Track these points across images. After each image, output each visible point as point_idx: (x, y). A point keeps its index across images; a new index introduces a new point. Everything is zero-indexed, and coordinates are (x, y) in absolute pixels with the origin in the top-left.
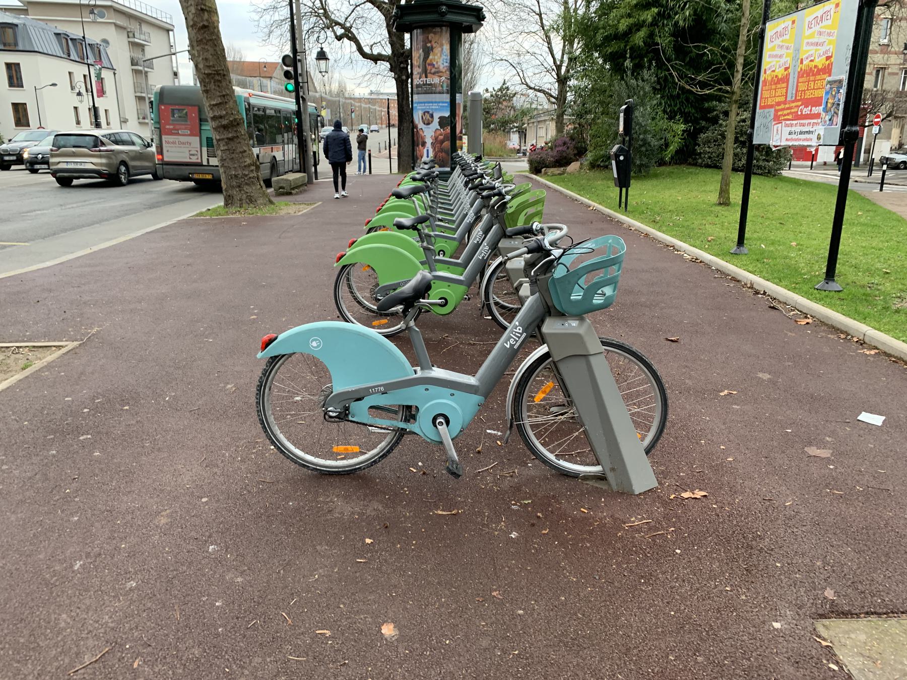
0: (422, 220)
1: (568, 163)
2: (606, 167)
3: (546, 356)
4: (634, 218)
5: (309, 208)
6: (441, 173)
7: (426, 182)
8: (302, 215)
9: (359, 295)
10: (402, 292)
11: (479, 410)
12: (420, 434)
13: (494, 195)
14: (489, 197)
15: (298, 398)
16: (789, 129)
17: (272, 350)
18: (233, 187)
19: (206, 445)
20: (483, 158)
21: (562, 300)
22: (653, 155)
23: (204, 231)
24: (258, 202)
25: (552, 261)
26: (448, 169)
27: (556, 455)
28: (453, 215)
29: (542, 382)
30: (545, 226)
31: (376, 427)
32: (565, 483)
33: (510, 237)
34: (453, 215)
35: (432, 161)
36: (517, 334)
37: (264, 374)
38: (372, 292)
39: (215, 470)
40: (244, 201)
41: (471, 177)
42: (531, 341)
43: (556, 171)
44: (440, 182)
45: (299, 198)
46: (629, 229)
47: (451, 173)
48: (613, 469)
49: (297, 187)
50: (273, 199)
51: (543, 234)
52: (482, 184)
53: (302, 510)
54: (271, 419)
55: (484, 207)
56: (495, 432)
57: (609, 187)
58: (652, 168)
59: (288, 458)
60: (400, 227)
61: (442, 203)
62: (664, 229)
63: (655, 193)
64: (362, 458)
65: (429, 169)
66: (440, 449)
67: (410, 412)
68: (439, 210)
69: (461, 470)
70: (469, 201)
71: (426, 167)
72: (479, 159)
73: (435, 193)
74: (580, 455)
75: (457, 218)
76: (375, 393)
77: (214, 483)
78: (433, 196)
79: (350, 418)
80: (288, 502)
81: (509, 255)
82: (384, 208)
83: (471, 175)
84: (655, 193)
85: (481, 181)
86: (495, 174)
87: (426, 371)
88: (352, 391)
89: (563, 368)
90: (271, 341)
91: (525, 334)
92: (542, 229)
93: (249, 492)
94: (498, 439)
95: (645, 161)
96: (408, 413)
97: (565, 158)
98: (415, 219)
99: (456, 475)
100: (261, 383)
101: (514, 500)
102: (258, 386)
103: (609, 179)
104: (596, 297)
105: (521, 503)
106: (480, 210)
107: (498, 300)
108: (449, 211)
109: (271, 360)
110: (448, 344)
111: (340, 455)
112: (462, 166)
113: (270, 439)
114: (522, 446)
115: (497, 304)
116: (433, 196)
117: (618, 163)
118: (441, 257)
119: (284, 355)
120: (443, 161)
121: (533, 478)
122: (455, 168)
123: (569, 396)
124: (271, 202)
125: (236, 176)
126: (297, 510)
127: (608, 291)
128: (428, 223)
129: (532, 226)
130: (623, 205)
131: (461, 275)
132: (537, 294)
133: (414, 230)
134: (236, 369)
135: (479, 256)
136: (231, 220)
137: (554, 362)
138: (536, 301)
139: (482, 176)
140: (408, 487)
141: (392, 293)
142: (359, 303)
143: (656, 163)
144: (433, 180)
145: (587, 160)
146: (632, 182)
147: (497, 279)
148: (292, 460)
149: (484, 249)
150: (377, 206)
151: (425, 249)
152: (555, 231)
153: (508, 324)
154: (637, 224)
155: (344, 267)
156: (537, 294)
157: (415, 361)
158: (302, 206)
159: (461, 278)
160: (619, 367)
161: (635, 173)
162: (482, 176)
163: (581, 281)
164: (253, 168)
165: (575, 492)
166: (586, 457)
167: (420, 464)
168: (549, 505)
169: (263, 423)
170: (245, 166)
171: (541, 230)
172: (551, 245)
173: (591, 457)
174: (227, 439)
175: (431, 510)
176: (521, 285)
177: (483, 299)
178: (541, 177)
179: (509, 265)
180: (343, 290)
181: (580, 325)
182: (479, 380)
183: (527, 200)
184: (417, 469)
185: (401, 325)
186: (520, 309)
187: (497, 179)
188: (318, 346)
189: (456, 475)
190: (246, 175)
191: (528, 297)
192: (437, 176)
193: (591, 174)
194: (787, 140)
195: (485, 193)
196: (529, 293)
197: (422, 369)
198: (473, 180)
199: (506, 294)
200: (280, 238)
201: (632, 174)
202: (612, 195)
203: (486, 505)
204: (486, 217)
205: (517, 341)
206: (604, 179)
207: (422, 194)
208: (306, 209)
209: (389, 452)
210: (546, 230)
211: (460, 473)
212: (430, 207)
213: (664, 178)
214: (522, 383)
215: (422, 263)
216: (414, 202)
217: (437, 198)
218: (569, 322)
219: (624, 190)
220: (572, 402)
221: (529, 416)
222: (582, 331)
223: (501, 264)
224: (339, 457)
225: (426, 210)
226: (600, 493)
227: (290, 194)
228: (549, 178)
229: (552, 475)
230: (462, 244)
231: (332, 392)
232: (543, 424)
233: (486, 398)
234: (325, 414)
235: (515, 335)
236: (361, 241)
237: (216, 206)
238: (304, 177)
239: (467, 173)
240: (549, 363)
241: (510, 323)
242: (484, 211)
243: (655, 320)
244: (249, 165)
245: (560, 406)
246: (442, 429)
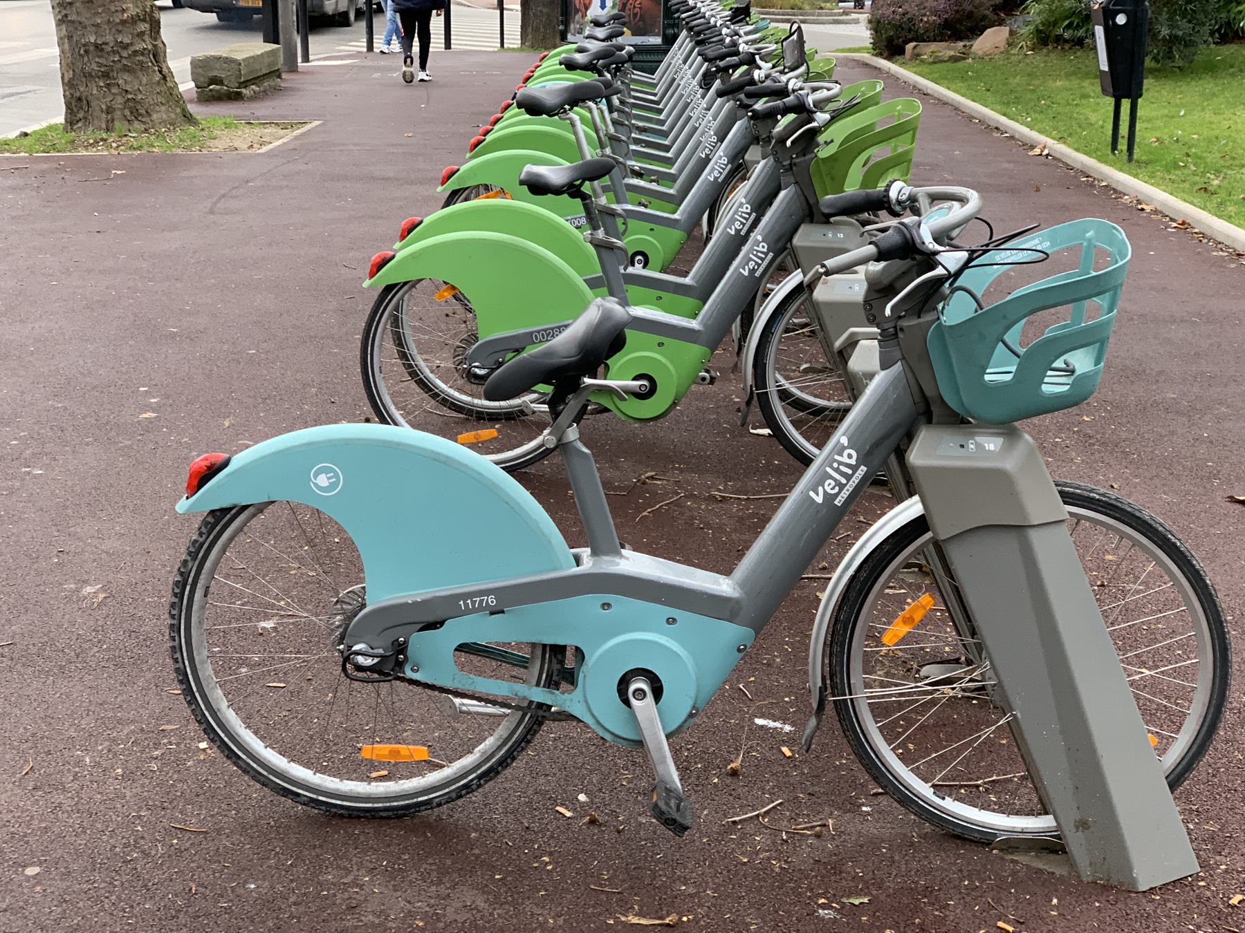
0: (596, 171)
1: (977, 30)
2: (1079, 42)
3: (918, 526)
4: (1151, 179)
5: (289, 136)
6: (640, 49)
7: (600, 74)
8: (269, 154)
9: (422, 364)
10: (548, 354)
11: (737, 669)
12: (588, 719)
13: (785, 111)
14: (770, 116)
15: (269, 624)
17: (216, 494)
18: (89, 76)
19: (34, 735)
20: (753, 10)
21: (960, 382)
22: (1206, 13)
23: (13, 189)
24: (155, 116)
25: (940, 281)
26: (656, 40)
27: (934, 786)
28: (670, 162)
29: (900, 602)
30: (921, 192)
31: (472, 697)
32: (959, 856)
33: (826, 219)
34: (670, 162)
35: (615, 18)
36: (843, 468)
37: (193, 555)
38: (460, 355)
39: (59, 798)
40: (118, 114)
41: (722, 64)
42: (872, 496)
43: (946, 49)
44: (638, 75)
45: (262, 109)
46: (1137, 207)
47: (663, 50)
48: (1082, 825)
49: (256, 80)
50: (192, 108)
51: (916, 212)
52: (752, 82)
53: (279, 902)
54: (207, 671)
55: (756, 140)
56: (778, 725)
57: (1085, 96)
58: (1203, 47)
59: (245, 771)
60: (538, 187)
61: (643, 130)
62: (1232, 209)
63: (1208, 115)
64: (434, 777)
65: (609, 38)
66: (634, 763)
67: (562, 662)
68: (633, 147)
69: (688, 813)
70: (715, 124)
71: (601, 33)
72: (741, 14)
73: (622, 102)
74: (998, 788)
75: (681, 170)
76: (474, 611)
77: (57, 830)
78: (619, 110)
79: (409, 674)
80: (246, 882)
81: (830, 263)
82: (489, 138)
83: (722, 58)
84: (1208, 115)
85: (748, 72)
86: (788, 55)
87: (606, 558)
88: (415, 603)
89: (958, 557)
90: (213, 470)
91: (863, 468)
92: (913, 199)
93: (145, 854)
94: (784, 743)
95: (1184, 28)
96: (556, 666)
97: (970, 15)
98: (575, 168)
99: (679, 828)
100: (184, 575)
101: (823, 895)
102: (177, 583)
103: (1086, 75)
104: (1051, 377)
105: (843, 905)
106: (744, 150)
107: (786, 385)
108: (658, 148)
109: (210, 519)
110: (655, 497)
111: (376, 769)
112: (698, 34)
113: (202, 720)
114: (846, 759)
115: (784, 395)
116: (619, 110)
117: (1111, 31)
118: (637, 269)
119: (245, 507)
120: (642, 18)
121: (875, 843)
122: (675, 37)
123: (973, 633)
124: (189, 118)
125: (98, 47)
126: (269, 903)
127: (1081, 361)
128: (606, 180)
129: (887, 190)
130: (1123, 145)
131: (695, 316)
132: (898, 367)
133: (573, 196)
134: (108, 545)
135: (740, 267)
136: (83, 163)
137: (938, 545)
138: (894, 384)
139: (750, 61)
140: (551, 854)
141: (531, 351)
142: (424, 385)
143: (1212, 34)
144: (618, 69)
145: (1027, 23)
146: (1148, 83)
147: (787, 331)
148: (256, 776)
149: (756, 252)
150: (473, 135)
151: (599, 246)
152: (947, 204)
153: (815, 450)
154: (1158, 195)
155: (389, 288)
156: (898, 367)
157: (576, 533)
158: (269, 130)
159: (694, 324)
160: (1103, 566)
161: (1155, 59)
162: (750, 61)
163: (1013, 336)
164: (144, 27)
165: (983, 881)
166: (1014, 793)
167: (582, 797)
168: (916, 910)
169: (184, 680)
170: (123, 22)
171: (912, 205)
172: (937, 239)
173: (1027, 795)
174: (87, 723)
175: (611, 914)
176: (852, 343)
177: (750, 380)
178: (902, 65)
179: (820, 294)
180: (384, 352)
181: (1007, 448)
182: (742, 585)
183: (871, 127)
184: (574, 810)
185: (546, 437)
186: (847, 411)
187: (793, 69)
188: (332, 486)
189: (679, 828)
190: (126, 47)
191: (871, 376)
192: (630, 55)
193: (1038, 59)
195: (760, 105)
196: (875, 363)
197: (595, 553)
198: (725, 70)
199: (806, 371)
200: (212, 212)
201: (1148, 62)
202: (1093, 118)
203: (751, 905)
204: (760, 167)
206: (1074, 73)
207: (591, 104)
208: (279, 139)
209: (504, 763)
210: (923, 203)
211: (687, 821)
212: (612, 138)
213: (1233, 75)
214: (853, 594)
215: (593, 284)
216: (573, 125)
217: (628, 116)
218: (979, 439)
219: (1126, 104)
220: (980, 647)
221: (867, 685)
222: (1009, 464)
223: (799, 289)
224: (374, 775)
225: (602, 147)
226: (1049, 883)
227: (234, 97)
228: (926, 69)
229: (924, 837)
230: (694, 240)
231: (363, 606)
232: (901, 705)
233: (757, 633)
234: (346, 659)
236: (431, 224)
237: (44, 125)
238: (273, 52)
239: (711, 51)
240: (919, 551)
241: (820, 446)
242: (753, 153)
243: (1202, 450)
244: (134, 20)
245: (948, 662)
246: (644, 707)
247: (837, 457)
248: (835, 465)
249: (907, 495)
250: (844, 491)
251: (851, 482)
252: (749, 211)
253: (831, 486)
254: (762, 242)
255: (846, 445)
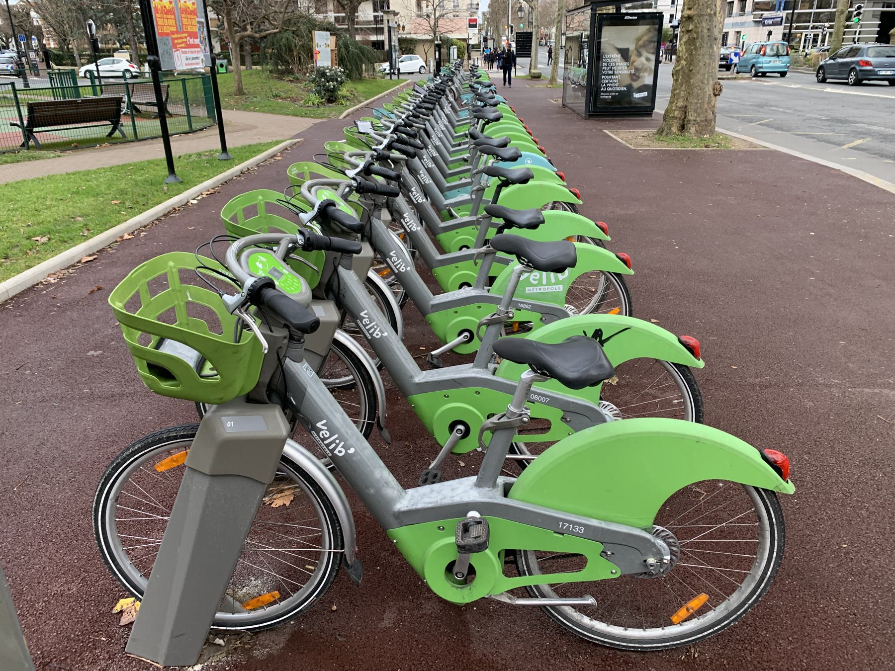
16: (185, 55)
36: (373, 330)
194: (186, 65)
205: (393, 263)
214: (366, 377)
235: (373, 327)
247: (342, 443)
248: (337, 441)
249: (409, 344)
250: (538, 288)
251: (546, 287)
252: (374, 335)
253: (535, 278)
254: (382, 335)
255: (348, 451)
